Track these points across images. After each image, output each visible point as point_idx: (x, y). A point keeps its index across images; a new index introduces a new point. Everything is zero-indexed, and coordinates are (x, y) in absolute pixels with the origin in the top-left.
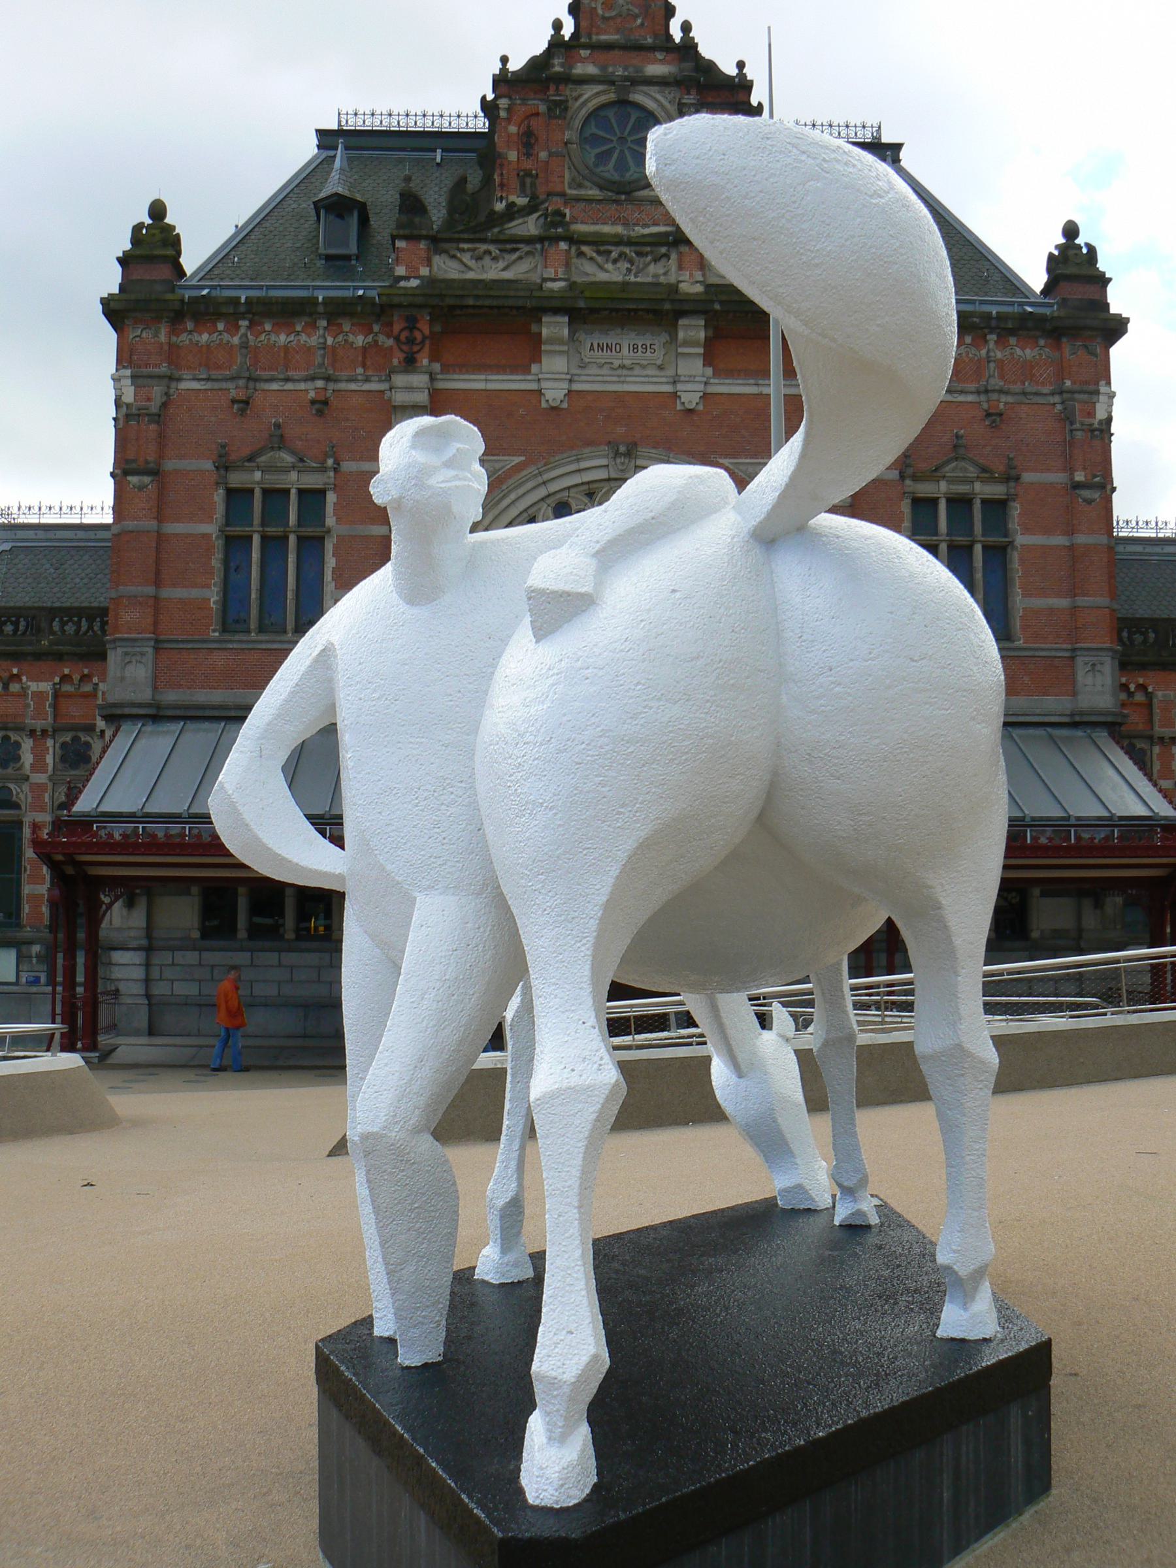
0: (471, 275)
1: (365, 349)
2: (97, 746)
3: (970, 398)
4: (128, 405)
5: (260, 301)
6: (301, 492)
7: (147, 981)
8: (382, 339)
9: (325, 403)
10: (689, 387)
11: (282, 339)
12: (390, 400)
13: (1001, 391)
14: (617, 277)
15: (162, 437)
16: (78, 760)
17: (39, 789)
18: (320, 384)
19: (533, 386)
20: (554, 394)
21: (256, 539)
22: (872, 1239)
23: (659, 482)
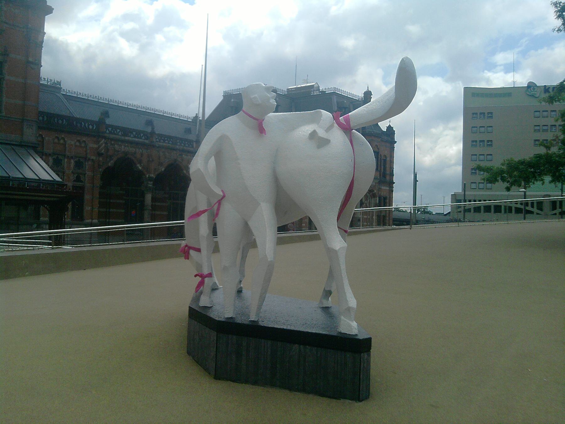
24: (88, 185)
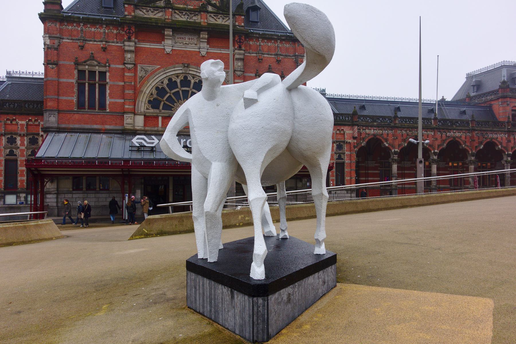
0: (145, 16)
1: (116, 34)
2: (40, 139)
3: (273, 56)
4: (48, 45)
5: (86, 18)
6: (99, 72)
7: (57, 202)
8: (121, 31)
9: (106, 48)
10: (203, 50)
11: (93, 29)
12: (124, 48)
13: (280, 55)
14: (185, 20)
15: (58, 55)
16: (34, 142)
17: (22, 151)
18: (104, 43)
19: (163, 47)
20: (168, 50)
21: (87, 84)
22: (288, 240)
23: (267, 77)
24: (347, 161)
